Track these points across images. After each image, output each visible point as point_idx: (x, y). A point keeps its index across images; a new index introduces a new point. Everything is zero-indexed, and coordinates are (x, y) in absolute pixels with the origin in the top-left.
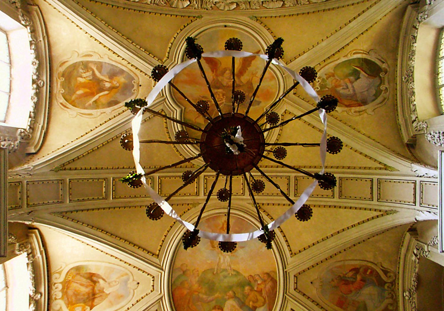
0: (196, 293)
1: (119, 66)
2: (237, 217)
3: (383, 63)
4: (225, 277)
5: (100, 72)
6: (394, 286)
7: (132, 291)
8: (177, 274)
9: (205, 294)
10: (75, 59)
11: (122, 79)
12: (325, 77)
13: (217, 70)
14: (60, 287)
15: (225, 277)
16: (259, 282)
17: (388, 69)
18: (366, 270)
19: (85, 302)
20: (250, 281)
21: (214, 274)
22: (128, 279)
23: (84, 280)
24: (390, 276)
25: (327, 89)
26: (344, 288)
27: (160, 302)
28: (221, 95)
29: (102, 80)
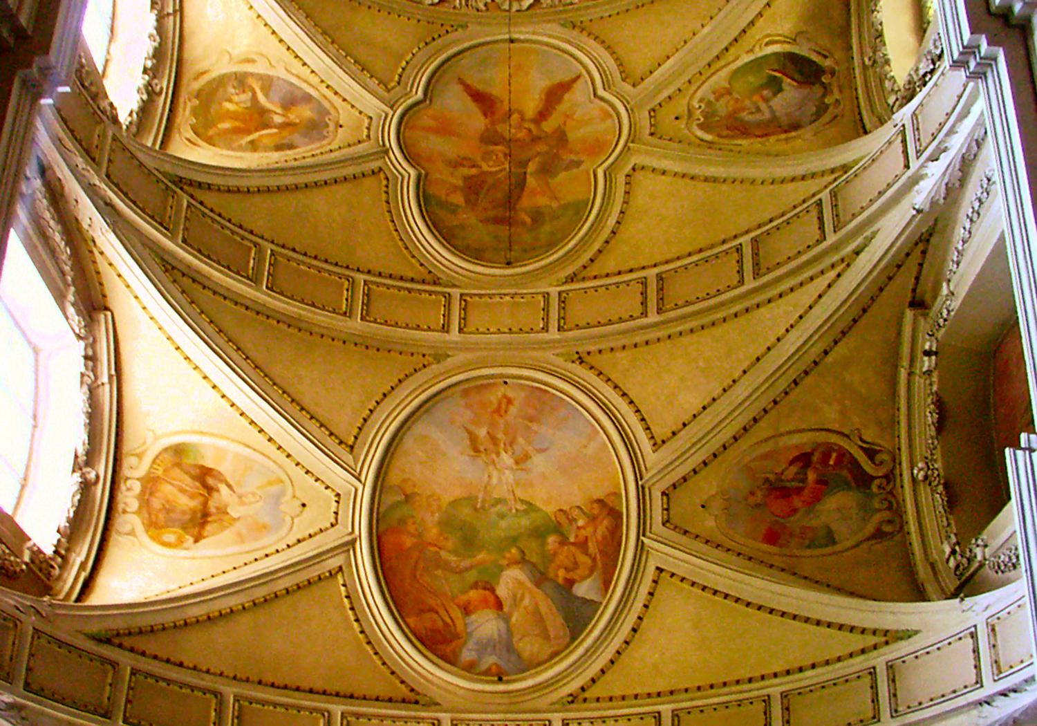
0: (434, 549)
1: (304, 86)
2: (532, 387)
3: (826, 57)
4: (502, 516)
5: (266, 95)
6: (892, 484)
7: (288, 520)
8: (390, 499)
9: (456, 553)
10: (222, 67)
11: (305, 112)
12: (712, 98)
13: (493, 113)
14: (137, 487)
15: (502, 516)
16: (581, 523)
17: (837, 68)
18: (826, 456)
19: (184, 528)
20: (559, 523)
21: (476, 509)
22: (283, 493)
23: (188, 480)
24: (881, 463)
25: (718, 118)
26: (778, 506)
27: (348, 550)
28: (501, 155)
29: (269, 111)
